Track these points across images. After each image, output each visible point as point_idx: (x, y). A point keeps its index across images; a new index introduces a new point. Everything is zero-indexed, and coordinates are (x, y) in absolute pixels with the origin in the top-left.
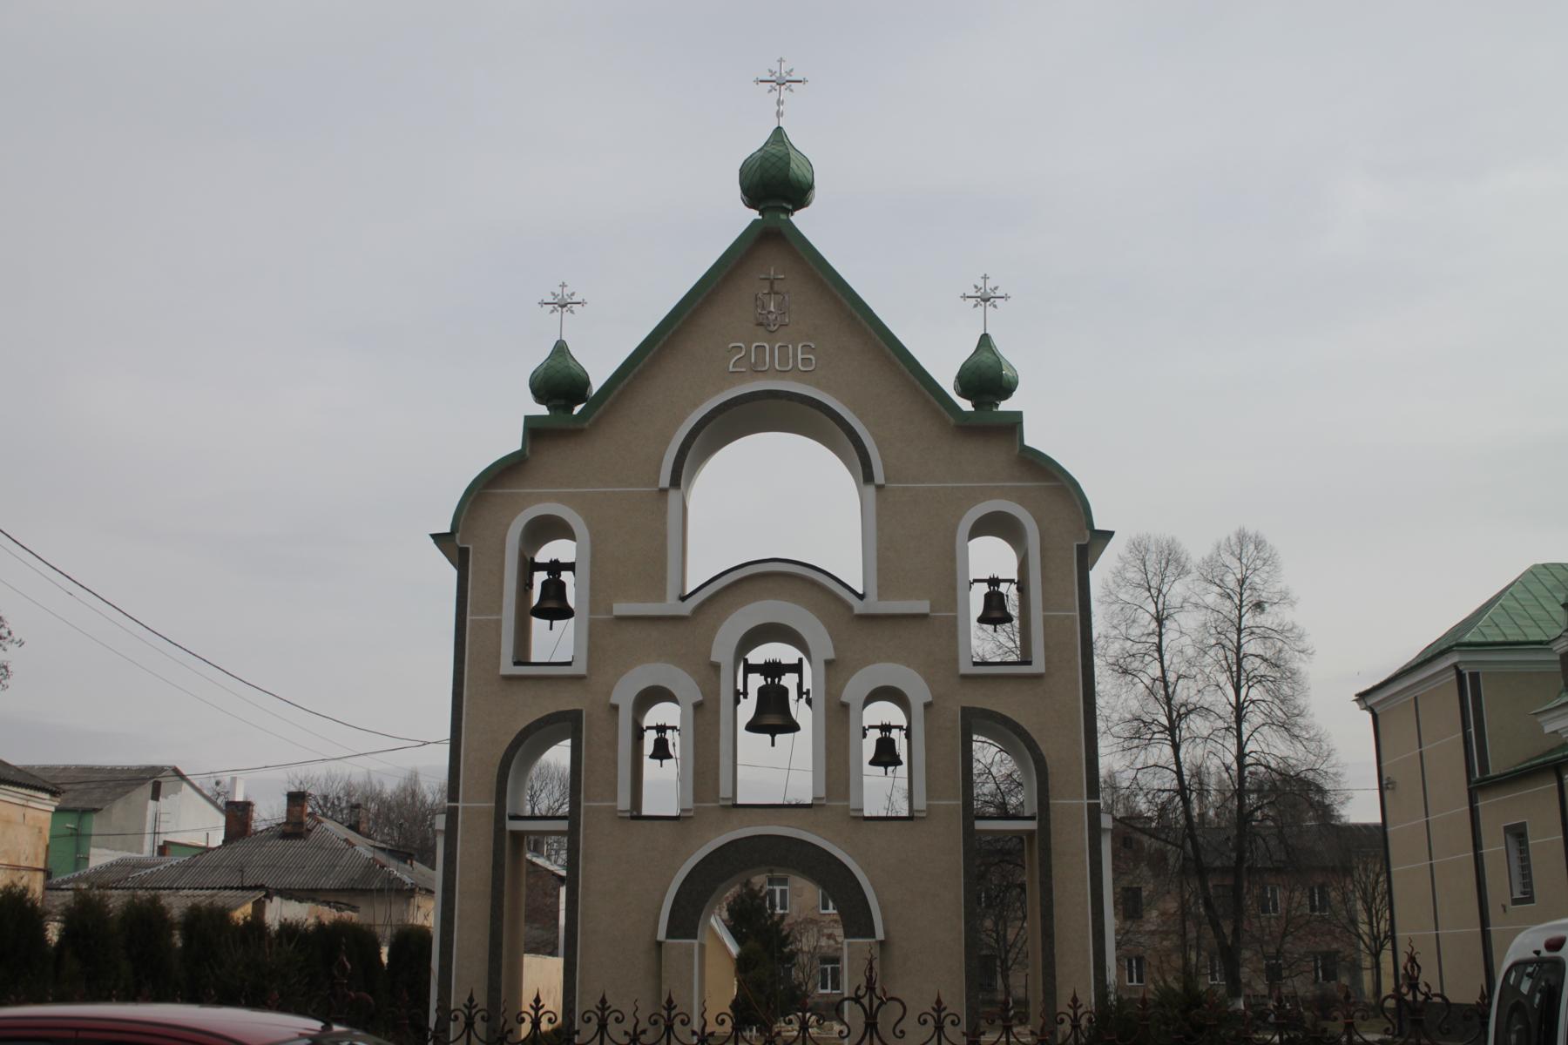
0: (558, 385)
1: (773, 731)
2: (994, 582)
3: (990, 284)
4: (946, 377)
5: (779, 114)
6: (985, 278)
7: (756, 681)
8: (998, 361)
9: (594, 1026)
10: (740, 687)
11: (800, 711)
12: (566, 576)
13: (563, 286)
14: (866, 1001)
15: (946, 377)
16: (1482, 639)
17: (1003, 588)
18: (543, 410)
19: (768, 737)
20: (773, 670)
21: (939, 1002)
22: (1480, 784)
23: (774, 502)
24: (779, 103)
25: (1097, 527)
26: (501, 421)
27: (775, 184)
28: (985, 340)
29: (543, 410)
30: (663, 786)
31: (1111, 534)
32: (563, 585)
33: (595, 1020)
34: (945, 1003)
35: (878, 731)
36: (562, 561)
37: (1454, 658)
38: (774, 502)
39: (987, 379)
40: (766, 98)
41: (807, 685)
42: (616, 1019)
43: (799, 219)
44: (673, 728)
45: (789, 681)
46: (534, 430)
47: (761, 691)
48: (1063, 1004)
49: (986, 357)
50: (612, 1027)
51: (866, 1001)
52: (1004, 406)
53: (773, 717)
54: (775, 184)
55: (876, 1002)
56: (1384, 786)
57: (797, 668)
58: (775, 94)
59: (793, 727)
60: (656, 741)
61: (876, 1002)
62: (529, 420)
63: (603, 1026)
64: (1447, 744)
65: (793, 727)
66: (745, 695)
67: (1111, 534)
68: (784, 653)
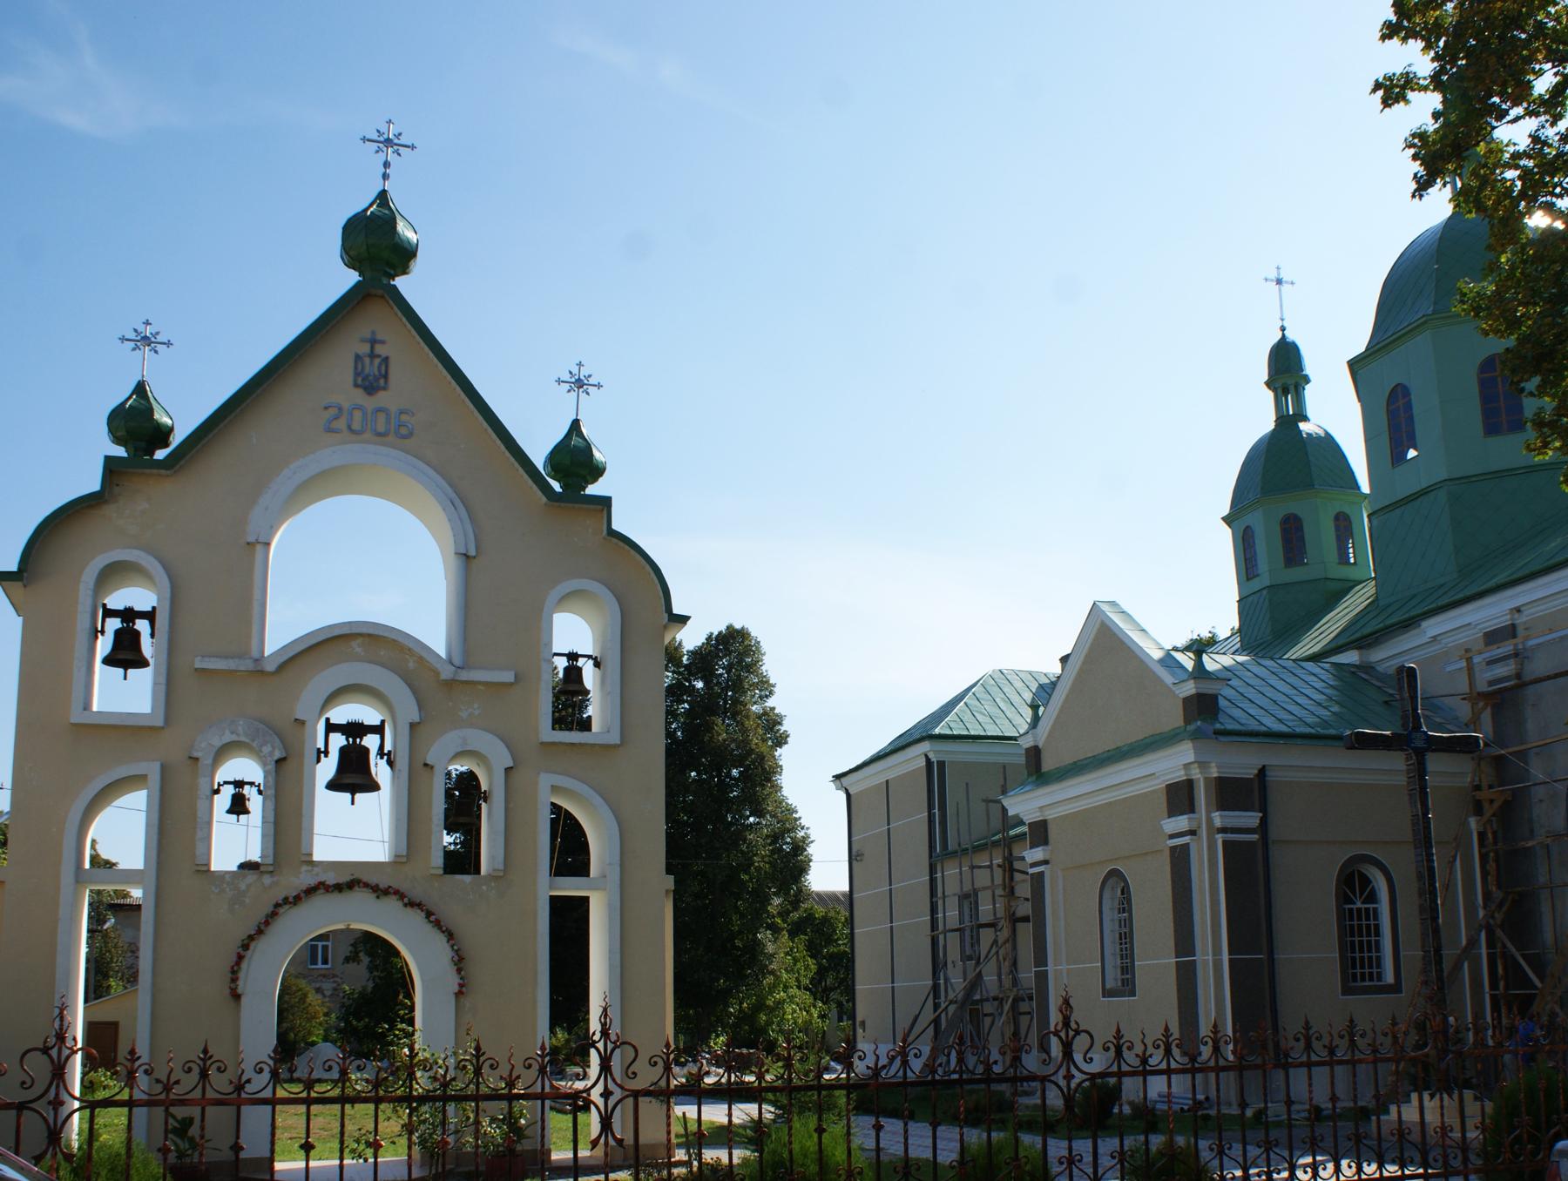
0: (136, 425)
1: (353, 789)
2: (573, 657)
3: (584, 372)
4: (539, 455)
5: (385, 177)
6: (580, 365)
7: (337, 740)
8: (587, 449)
9: (1302, 1044)
10: (321, 745)
11: (380, 770)
12: (142, 626)
13: (580, 365)
14: (1063, 1034)
15: (539, 455)
16: (948, 732)
17: (581, 662)
18: (120, 452)
19: (348, 796)
20: (355, 730)
21: (1118, 1031)
22: (939, 852)
23: (361, 561)
24: (386, 164)
25: (14, 568)
26: (80, 461)
27: (376, 245)
28: (576, 425)
29: (120, 452)
30: (234, 842)
31: (688, 618)
32: (138, 634)
33: (196, 1070)
34: (211, 1051)
35: (231, 787)
36: (136, 609)
37: (925, 747)
38: (361, 561)
39: (576, 460)
40: (373, 161)
41: (388, 747)
42: (219, 1069)
43: (400, 282)
44: (252, 784)
45: (371, 742)
46: (112, 468)
47: (342, 750)
48: (1205, 1030)
49: (575, 441)
50: (1126, 1054)
51: (1063, 1034)
52: (591, 490)
53: (353, 776)
54: (376, 245)
55: (1071, 1033)
56: (853, 857)
57: (379, 730)
58: (381, 157)
59: (373, 786)
60: (234, 796)
61: (1071, 1033)
62: (108, 459)
63: (204, 1075)
64: (913, 820)
65: (373, 786)
66: (326, 753)
67: (688, 618)
68: (368, 714)
